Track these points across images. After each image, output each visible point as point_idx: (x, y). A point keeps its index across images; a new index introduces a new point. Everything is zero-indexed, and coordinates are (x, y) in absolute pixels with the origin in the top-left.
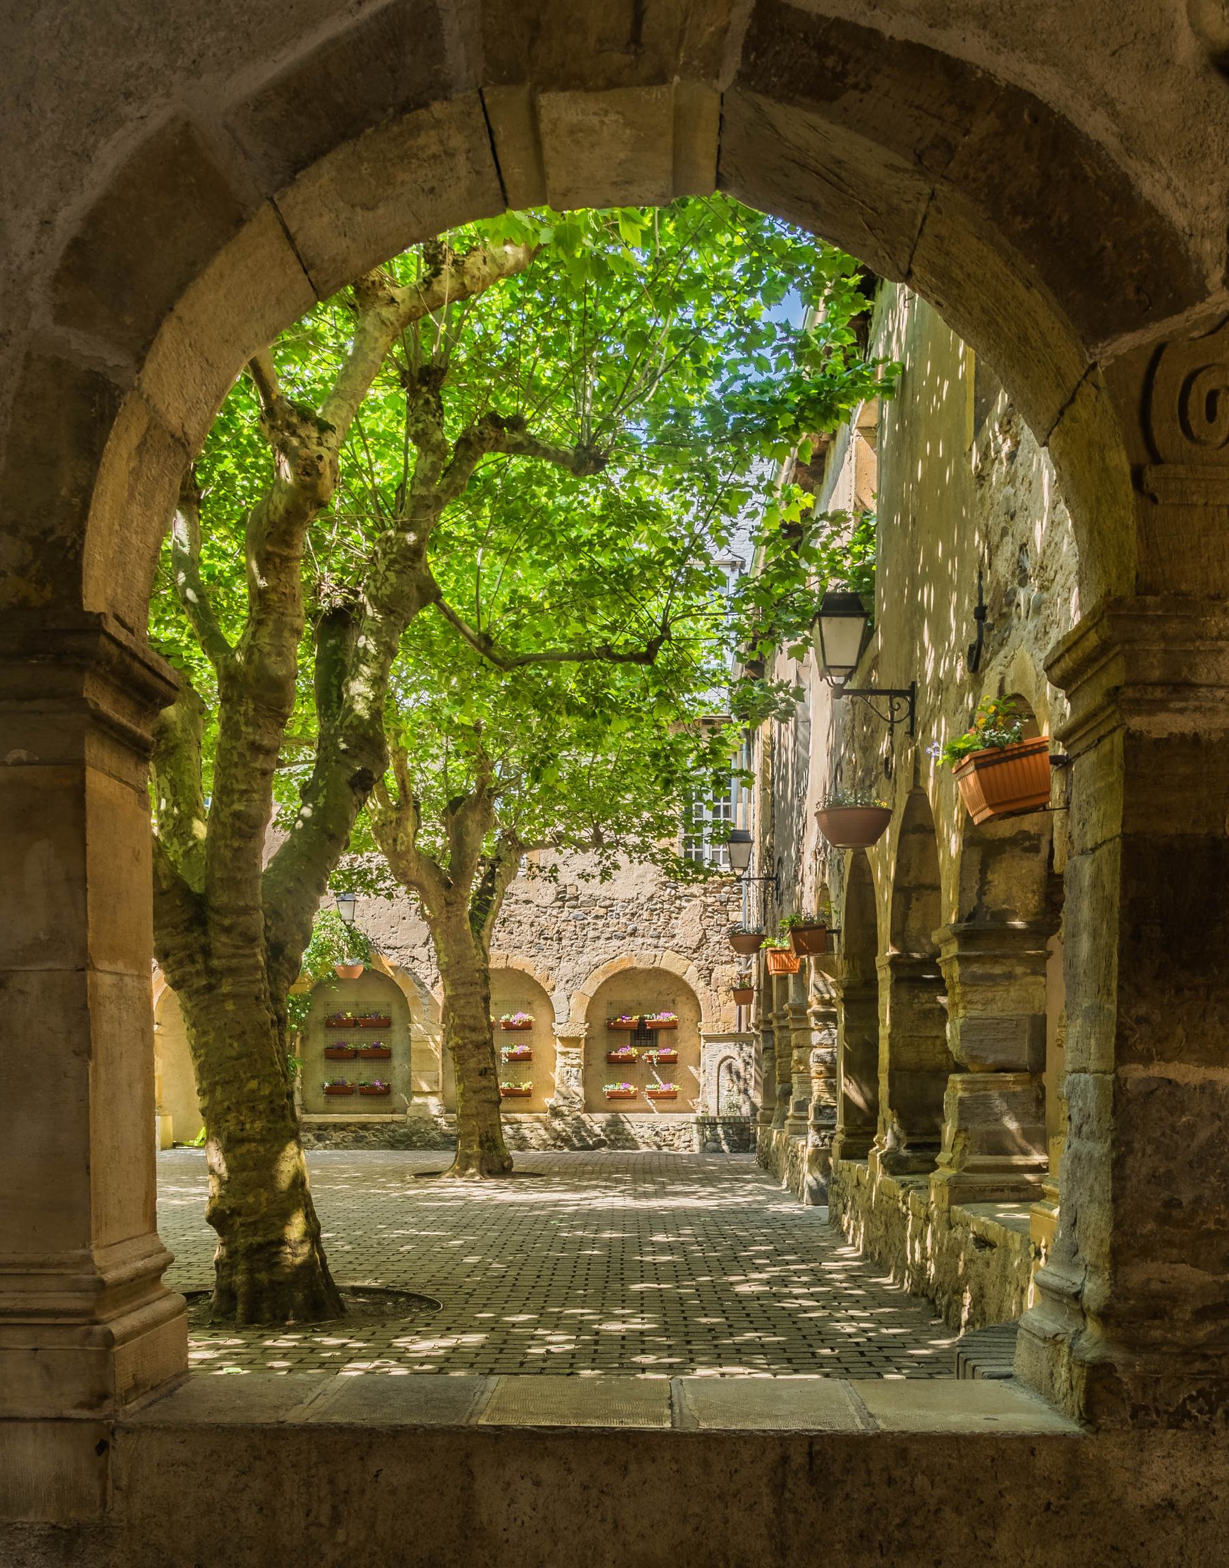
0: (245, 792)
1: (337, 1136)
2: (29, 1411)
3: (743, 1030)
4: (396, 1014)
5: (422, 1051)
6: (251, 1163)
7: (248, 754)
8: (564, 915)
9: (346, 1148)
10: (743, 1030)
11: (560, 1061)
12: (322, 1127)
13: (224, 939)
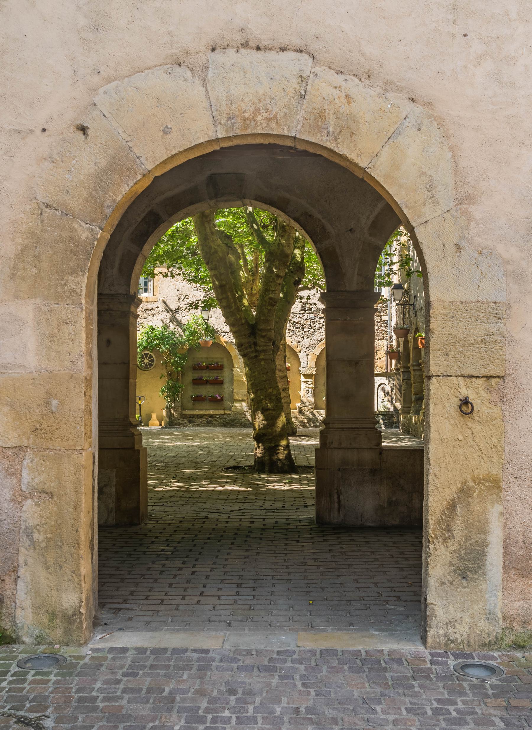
0: (274, 291)
1: (198, 421)
2: (365, 447)
3: (389, 371)
4: (226, 363)
5: (239, 381)
6: (270, 418)
7: (276, 278)
8: (305, 317)
9: (203, 426)
10: (389, 371)
11: (303, 385)
12: (192, 416)
13: (262, 340)
